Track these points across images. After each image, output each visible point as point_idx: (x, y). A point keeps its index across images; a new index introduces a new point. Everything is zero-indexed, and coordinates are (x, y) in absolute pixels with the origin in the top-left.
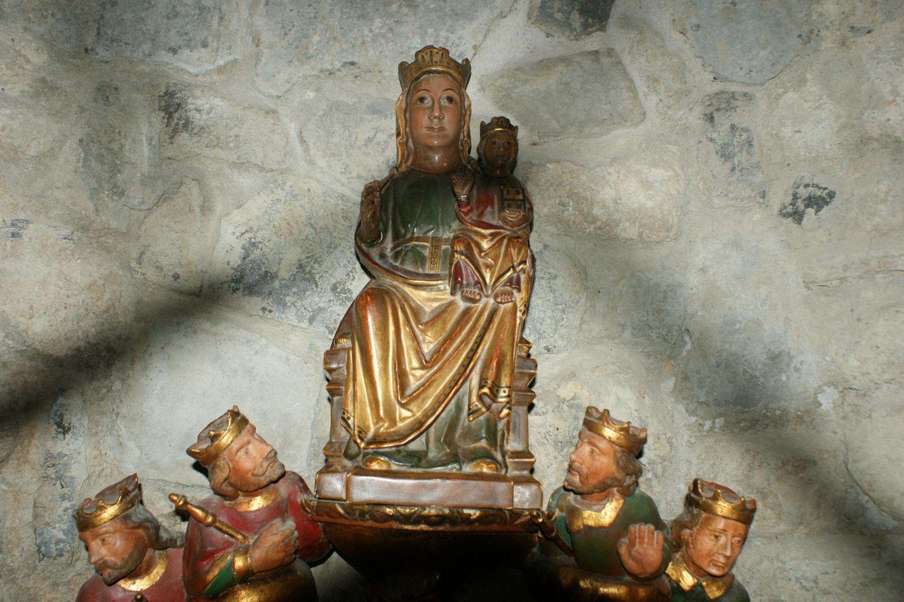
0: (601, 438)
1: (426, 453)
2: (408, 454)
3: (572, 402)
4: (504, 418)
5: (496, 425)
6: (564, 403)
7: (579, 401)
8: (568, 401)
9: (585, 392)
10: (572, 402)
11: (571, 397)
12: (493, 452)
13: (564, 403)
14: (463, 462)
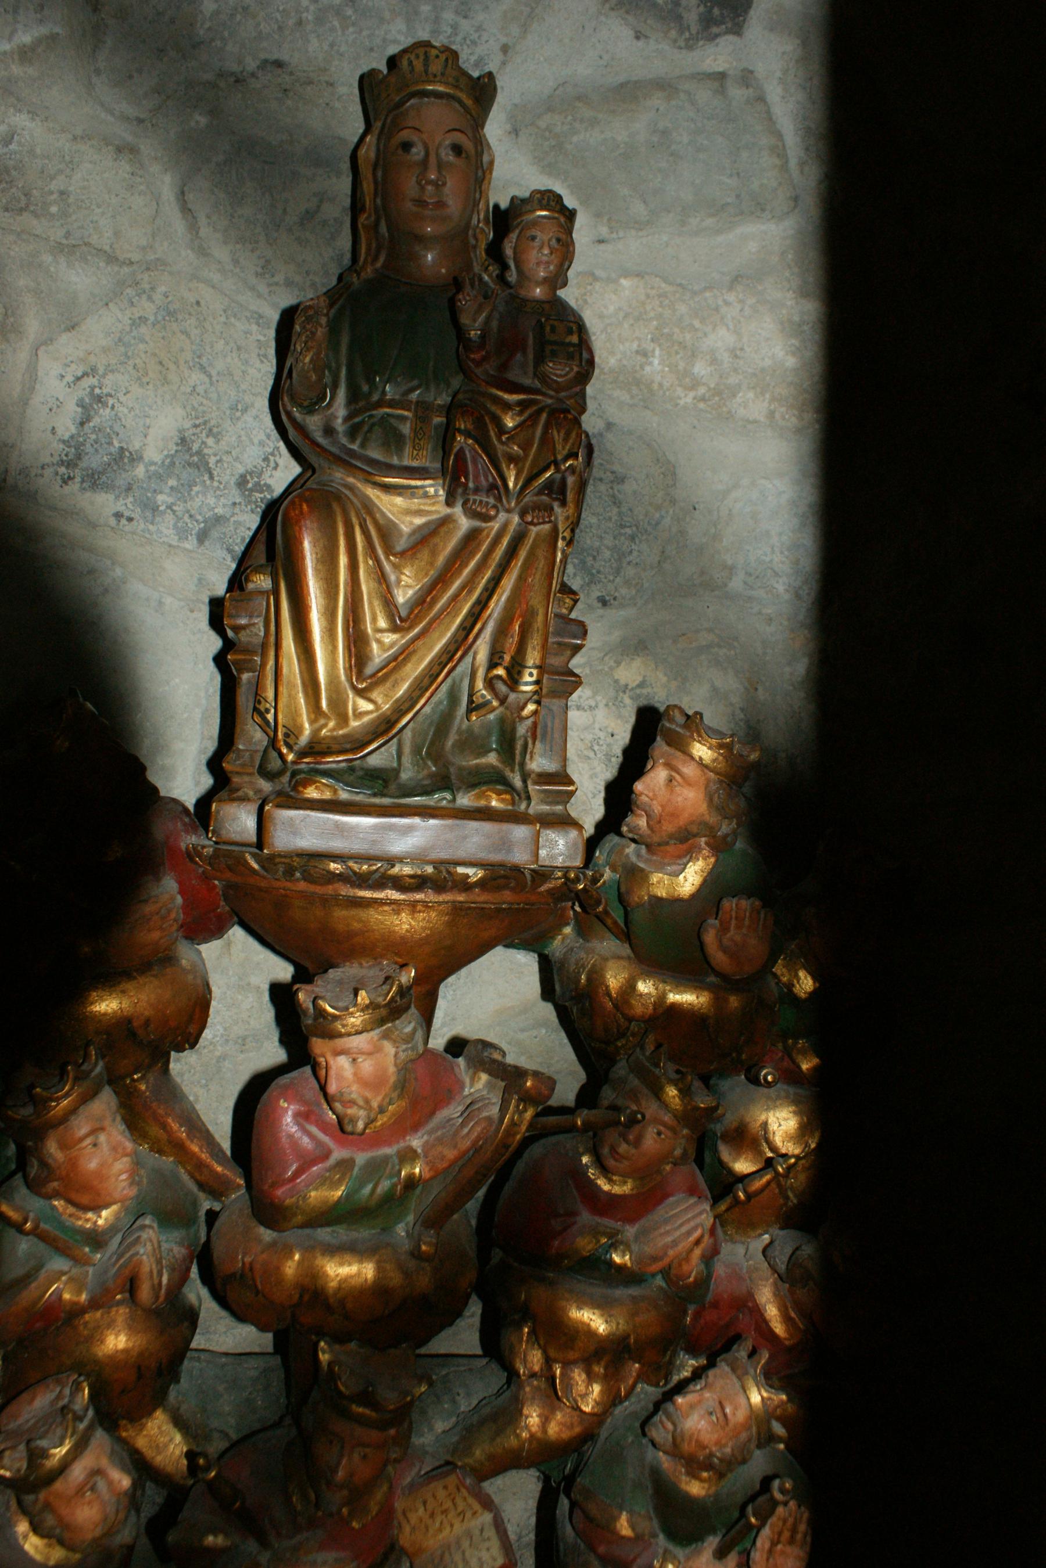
0: (688, 758)
1: (397, 771)
2: (366, 774)
3: (638, 691)
4: (528, 718)
5: (514, 730)
6: (624, 692)
7: (649, 690)
8: (632, 689)
9: (661, 675)
10: (638, 691)
11: (637, 682)
12: (508, 773)
13: (624, 692)
14: (459, 789)
